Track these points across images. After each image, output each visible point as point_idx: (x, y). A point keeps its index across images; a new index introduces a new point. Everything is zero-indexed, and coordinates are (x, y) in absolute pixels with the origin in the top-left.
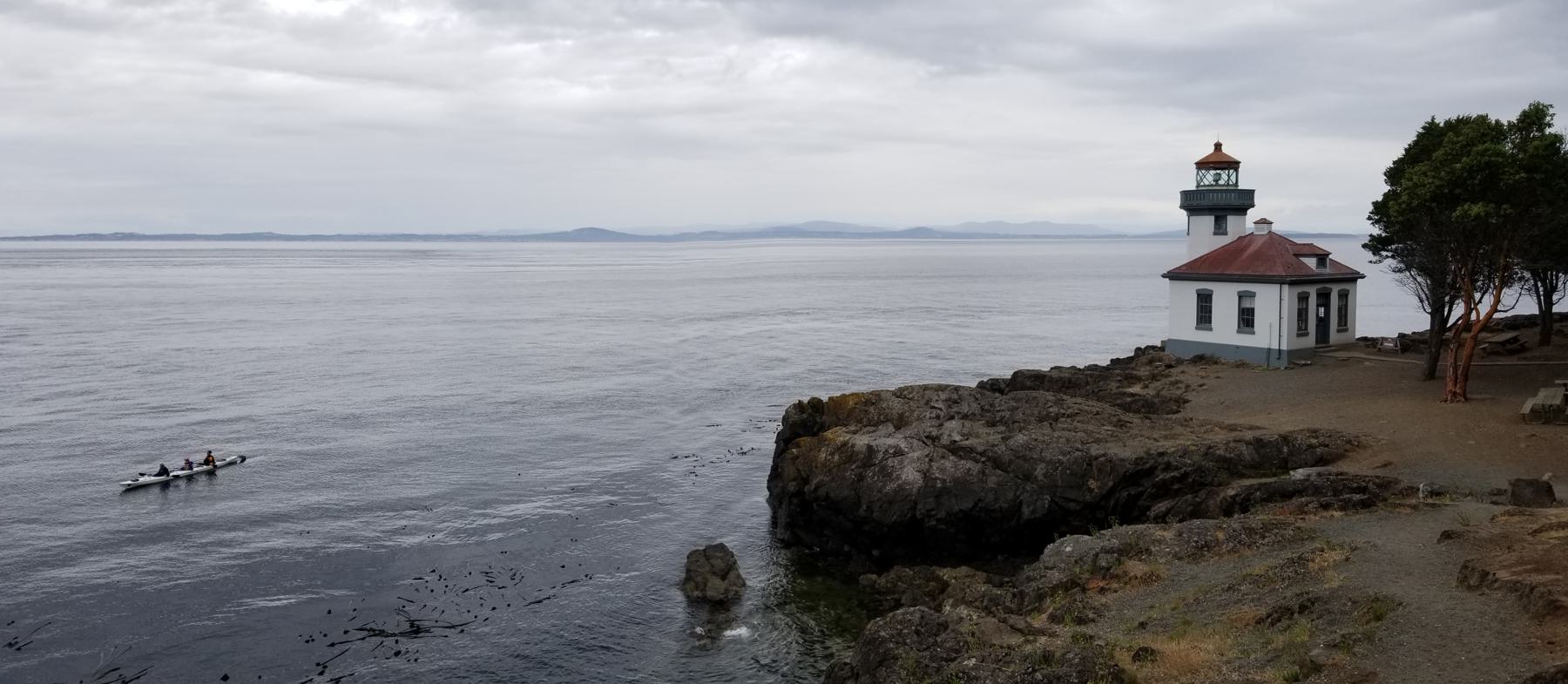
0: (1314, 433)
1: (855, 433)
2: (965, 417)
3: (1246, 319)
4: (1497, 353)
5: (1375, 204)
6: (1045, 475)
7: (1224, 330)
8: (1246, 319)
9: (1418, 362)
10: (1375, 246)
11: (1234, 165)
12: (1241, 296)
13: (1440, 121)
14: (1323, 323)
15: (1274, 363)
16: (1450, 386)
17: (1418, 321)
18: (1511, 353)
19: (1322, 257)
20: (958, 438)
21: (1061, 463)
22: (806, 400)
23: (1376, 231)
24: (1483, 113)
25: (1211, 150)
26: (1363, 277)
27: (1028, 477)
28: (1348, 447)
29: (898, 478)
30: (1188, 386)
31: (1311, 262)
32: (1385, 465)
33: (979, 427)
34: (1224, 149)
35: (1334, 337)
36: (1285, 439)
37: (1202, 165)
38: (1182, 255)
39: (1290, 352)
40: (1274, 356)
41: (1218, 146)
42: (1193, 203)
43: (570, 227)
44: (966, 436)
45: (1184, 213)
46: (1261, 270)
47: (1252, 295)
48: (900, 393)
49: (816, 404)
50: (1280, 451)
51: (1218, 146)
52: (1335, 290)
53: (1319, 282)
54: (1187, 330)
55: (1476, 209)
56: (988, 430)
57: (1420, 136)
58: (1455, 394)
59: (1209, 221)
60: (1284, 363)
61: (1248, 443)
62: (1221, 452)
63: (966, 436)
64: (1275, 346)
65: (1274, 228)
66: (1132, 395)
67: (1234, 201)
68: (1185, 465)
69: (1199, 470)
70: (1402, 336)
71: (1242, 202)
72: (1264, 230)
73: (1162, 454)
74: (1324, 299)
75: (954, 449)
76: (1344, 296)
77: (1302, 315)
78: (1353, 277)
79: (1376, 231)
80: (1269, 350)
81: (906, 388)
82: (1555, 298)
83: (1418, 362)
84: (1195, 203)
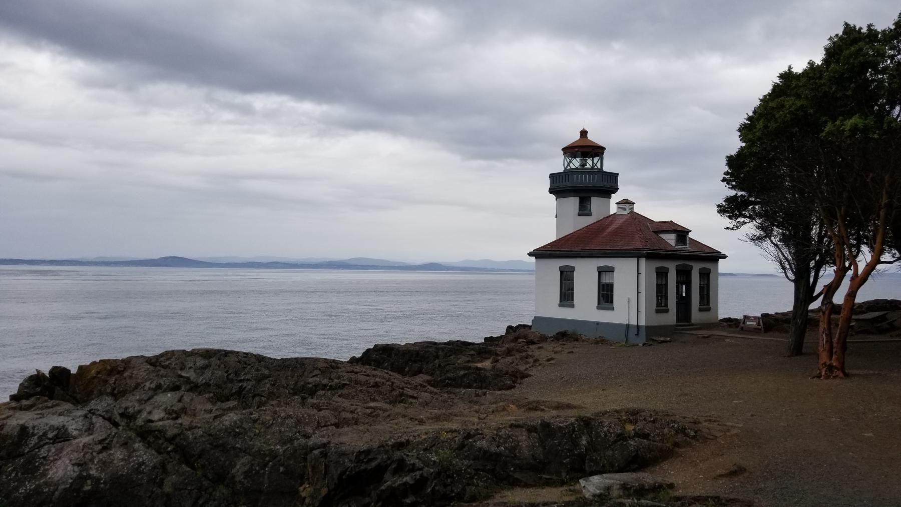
0: (634, 415)
3: (606, 296)
4: (867, 332)
5: (731, 161)
6: (246, 474)
7: (585, 308)
8: (606, 296)
9: (783, 340)
10: (732, 209)
11: (597, 151)
12: (601, 271)
14: (684, 303)
15: (632, 338)
16: (824, 357)
17: (781, 299)
18: (881, 332)
21: (273, 455)
22: (46, 369)
25: (577, 137)
26: (724, 257)
27: (222, 477)
28: (680, 438)
30: (536, 361)
31: (671, 239)
32: (733, 474)
33: (201, 405)
34: (590, 136)
35: (696, 316)
36: (586, 423)
37: (570, 151)
38: (548, 235)
39: (648, 328)
40: (633, 332)
41: (584, 133)
42: (561, 186)
43: (156, 255)
45: (553, 197)
46: (620, 245)
47: (611, 270)
50: (575, 443)
51: (584, 133)
54: (553, 310)
58: (830, 368)
59: (573, 203)
60: (642, 339)
61: (531, 430)
62: (483, 444)
64: (634, 322)
65: (636, 209)
67: (595, 180)
68: (427, 463)
69: (444, 472)
70: (765, 316)
71: (608, 185)
74: (684, 276)
76: (705, 275)
77: (661, 290)
78: (715, 257)
80: (628, 325)
83: (783, 340)
84: (560, 185)
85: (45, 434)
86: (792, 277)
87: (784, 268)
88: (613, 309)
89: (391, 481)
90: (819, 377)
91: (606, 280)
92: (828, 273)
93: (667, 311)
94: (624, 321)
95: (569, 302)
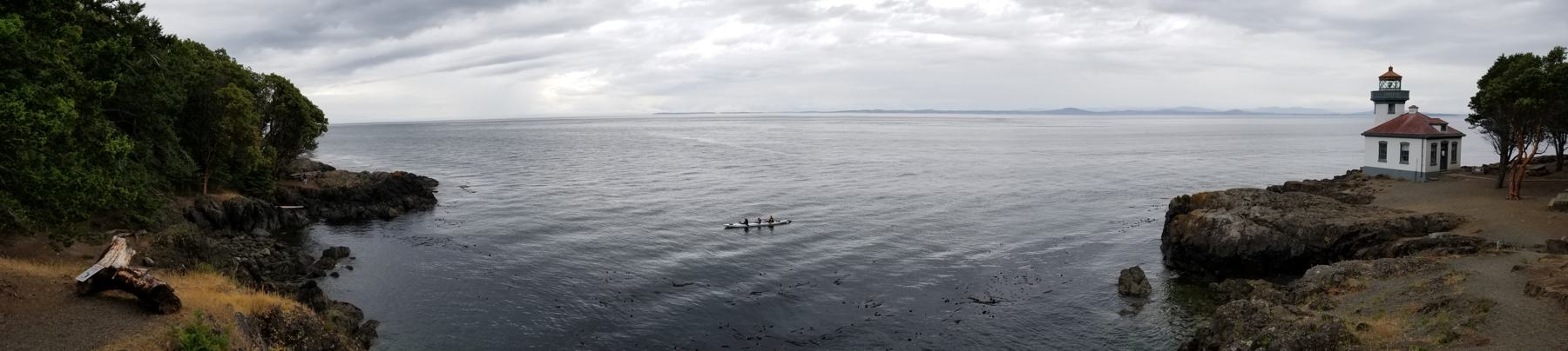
0: (1441, 215)
3: (1405, 157)
7: (1393, 162)
8: (1405, 157)
9: (1494, 179)
10: (1472, 120)
11: (1399, 78)
12: (1402, 145)
14: (1444, 159)
23: (1473, 112)
27: (1294, 235)
31: (1438, 128)
35: (1450, 166)
37: (1382, 78)
38: (1372, 124)
39: (1428, 174)
42: (1377, 98)
43: (1061, 107)
46: (1413, 131)
49: (1186, 198)
52: (1450, 142)
53: (1442, 138)
54: (1373, 161)
55: (1526, 101)
59: (1385, 107)
67: (1398, 96)
74: (1444, 146)
75: (1256, 220)
76: (1455, 145)
77: (1433, 155)
78: (1460, 136)
79: (1473, 112)
83: (1494, 179)
89: (1362, 236)
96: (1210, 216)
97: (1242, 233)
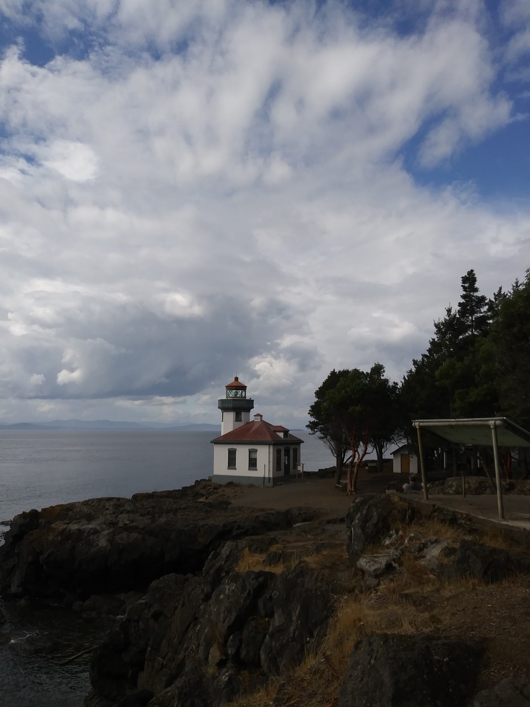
1: (68, 524)
2: (129, 512)
3: (253, 464)
7: (242, 469)
8: (253, 464)
10: (312, 426)
11: (244, 388)
12: (251, 452)
13: (337, 371)
14: (287, 467)
15: (267, 484)
19: (286, 432)
20: (128, 522)
23: (312, 419)
24: (384, 365)
26: (303, 442)
29: (97, 545)
31: (281, 435)
35: (292, 471)
37: (230, 388)
41: (236, 379)
44: (132, 521)
48: (86, 503)
49: (34, 513)
52: (292, 447)
53: (286, 446)
55: (358, 408)
56: (142, 518)
57: (329, 377)
58: (351, 491)
63: (132, 521)
64: (267, 476)
66: (201, 502)
72: (258, 419)
73: (235, 522)
75: (126, 528)
78: (299, 442)
79: (312, 419)
80: (264, 478)
81: (89, 500)
82: (383, 450)
84: (226, 406)
85: (89, 531)
86: (336, 455)
87: (332, 451)
88: (257, 470)
90: (347, 495)
91: (253, 456)
92: (349, 453)
93: (281, 470)
94: (262, 476)
95: (233, 467)
96: (74, 527)
97: (111, 541)
